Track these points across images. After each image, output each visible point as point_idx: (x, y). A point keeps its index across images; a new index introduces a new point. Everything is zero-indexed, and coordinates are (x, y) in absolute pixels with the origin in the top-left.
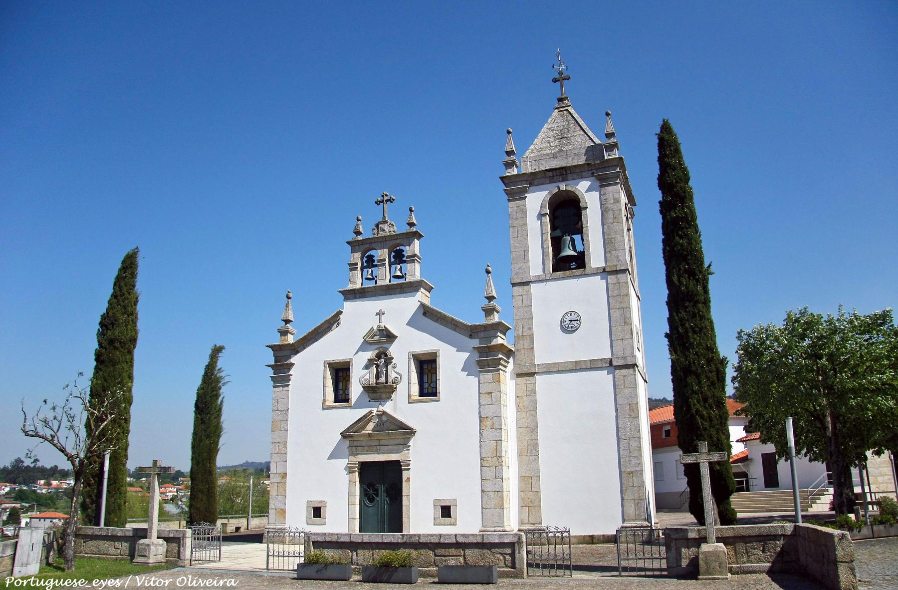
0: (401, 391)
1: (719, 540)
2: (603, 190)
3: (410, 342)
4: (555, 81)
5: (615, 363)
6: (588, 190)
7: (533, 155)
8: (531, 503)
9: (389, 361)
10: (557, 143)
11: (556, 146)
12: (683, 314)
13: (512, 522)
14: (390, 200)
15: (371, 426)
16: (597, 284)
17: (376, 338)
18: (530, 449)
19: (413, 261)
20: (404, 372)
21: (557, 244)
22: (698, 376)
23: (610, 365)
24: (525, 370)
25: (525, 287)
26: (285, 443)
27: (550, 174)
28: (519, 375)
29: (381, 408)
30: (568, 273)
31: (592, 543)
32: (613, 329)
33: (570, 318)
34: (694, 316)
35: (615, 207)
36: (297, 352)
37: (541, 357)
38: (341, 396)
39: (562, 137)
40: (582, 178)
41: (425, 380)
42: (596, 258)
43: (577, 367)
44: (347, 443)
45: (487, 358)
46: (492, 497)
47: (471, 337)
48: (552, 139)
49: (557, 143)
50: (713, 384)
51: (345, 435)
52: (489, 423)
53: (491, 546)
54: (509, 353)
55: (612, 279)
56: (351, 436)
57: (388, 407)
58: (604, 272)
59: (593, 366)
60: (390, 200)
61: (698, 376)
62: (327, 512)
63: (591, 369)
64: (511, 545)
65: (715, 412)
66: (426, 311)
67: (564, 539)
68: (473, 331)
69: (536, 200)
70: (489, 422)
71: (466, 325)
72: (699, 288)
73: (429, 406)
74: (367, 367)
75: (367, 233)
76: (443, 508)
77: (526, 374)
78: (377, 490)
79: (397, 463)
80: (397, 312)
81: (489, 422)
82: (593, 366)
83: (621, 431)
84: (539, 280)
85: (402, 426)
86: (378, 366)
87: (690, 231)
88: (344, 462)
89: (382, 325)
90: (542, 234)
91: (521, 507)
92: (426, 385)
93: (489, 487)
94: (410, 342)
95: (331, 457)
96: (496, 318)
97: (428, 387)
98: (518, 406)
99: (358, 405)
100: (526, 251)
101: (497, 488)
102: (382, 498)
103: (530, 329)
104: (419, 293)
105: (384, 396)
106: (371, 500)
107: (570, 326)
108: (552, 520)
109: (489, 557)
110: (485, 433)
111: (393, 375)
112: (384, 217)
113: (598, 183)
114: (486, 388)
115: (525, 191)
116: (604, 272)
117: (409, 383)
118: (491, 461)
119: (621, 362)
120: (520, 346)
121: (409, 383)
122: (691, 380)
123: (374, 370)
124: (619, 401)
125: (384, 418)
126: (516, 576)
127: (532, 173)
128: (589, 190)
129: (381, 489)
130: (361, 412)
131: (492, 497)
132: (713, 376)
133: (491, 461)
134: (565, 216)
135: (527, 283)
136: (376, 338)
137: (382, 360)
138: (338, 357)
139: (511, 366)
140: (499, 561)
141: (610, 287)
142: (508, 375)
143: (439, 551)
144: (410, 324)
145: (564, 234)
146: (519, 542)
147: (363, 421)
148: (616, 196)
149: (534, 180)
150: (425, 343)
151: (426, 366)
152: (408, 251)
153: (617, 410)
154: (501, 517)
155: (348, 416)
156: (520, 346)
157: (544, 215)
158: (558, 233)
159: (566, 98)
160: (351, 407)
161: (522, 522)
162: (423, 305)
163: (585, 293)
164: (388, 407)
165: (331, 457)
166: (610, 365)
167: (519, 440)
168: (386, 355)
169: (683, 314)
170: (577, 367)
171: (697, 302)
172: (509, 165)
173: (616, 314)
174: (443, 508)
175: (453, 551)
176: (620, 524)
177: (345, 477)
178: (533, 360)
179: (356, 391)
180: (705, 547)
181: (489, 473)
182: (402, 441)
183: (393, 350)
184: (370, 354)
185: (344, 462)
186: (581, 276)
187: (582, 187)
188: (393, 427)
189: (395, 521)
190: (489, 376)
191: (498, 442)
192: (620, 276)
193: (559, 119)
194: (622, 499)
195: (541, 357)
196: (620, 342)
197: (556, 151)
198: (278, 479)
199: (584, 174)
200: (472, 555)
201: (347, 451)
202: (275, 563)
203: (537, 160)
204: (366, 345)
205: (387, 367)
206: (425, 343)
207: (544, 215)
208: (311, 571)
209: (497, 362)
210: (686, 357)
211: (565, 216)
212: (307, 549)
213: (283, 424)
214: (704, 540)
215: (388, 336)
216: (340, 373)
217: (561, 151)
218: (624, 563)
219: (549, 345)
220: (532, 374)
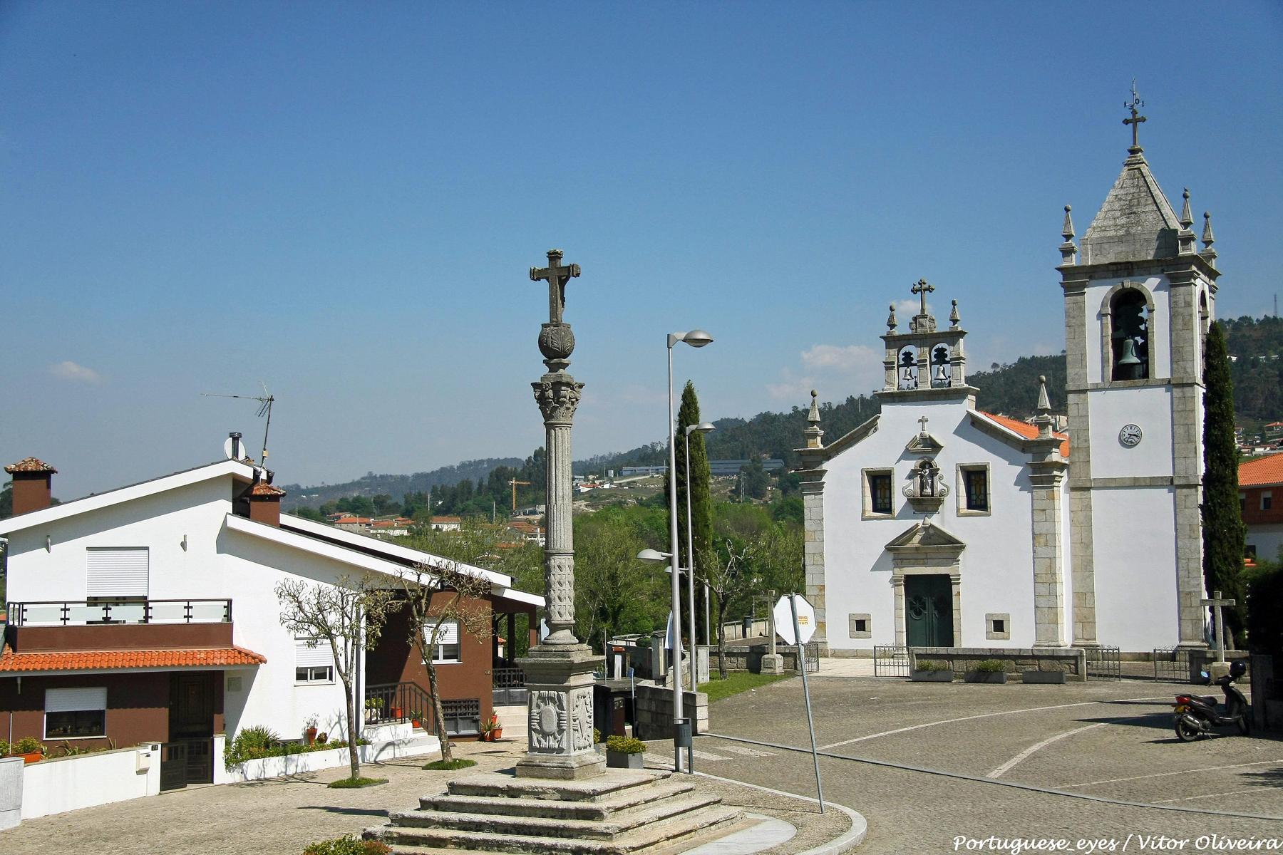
0: (949, 503)
1: (1227, 660)
2: (1174, 291)
3: (958, 453)
4: (1126, 122)
5: (1176, 482)
6: (1157, 289)
7: (1095, 236)
8: (1085, 618)
9: (934, 472)
10: (1124, 220)
11: (1122, 226)
12: (1213, 492)
13: (1066, 639)
14: (930, 289)
15: (917, 538)
16: (1161, 397)
17: (919, 447)
18: (1084, 566)
19: (958, 364)
20: (951, 483)
21: (1119, 350)
22: (1221, 541)
23: (1170, 484)
24: (1080, 484)
25: (1082, 396)
26: (822, 555)
27: (1114, 268)
28: (1073, 489)
29: (929, 521)
30: (1129, 382)
31: (1148, 660)
32: (1177, 446)
33: (1129, 431)
34: (1222, 493)
35: (1186, 312)
36: (829, 458)
37: (1098, 471)
38: (882, 504)
39: (1130, 210)
40: (1150, 274)
41: (973, 491)
42: (1161, 367)
43: (1136, 484)
44: (891, 555)
45: (1039, 475)
46: (1046, 613)
47: (1023, 451)
48: (1118, 214)
49: (1124, 220)
50: (1233, 546)
51: (890, 548)
52: (1042, 540)
53: (1059, 658)
54: (1061, 467)
55: (1177, 392)
56: (896, 551)
57: (934, 520)
58: (1169, 384)
59: (1153, 483)
60: (930, 289)
61: (1221, 541)
62: (873, 625)
63: (1150, 486)
64: (1075, 658)
65: (1233, 568)
66: (973, 421)
67: (1117, 656)
68: (1025, 446)
69: (1097, 296)
70: (1042, 539)
71: (1019, 440)
72: (1228, 472)
73: (978, 522)
74: (910, 477)
75: (902, 329)
76: (995, 622)
77: (1081, 488)
78: (924, 604)
79: (947, 576)
80: (943, 420)
81: (1042, 539)
82: (1153, 483)
83: (1180, 551)
84: (1097, 389)
85: (951, 541)
86: (922, 476)
87: (1225, 425)
88: (888, 575)
89: (927, 433)
90: (1102, 337)
91: (1075, 623)
92: (974, 497)
93: (1043, 603)
94: (958, 453)
95: (875, 568)
96: (1050, 435)
97: (977, 497)
98: (1072, 521)
99: (902, 516)
100: (1084, 355)
101: (1051, 604)
102: (931, 611)
103: (1087, 441)
104: (966, 401)
105: (930, 508)
106: (918, 613)
107: (1130, 440)
108: (1105, 638)
109: (1058, 666)
110: (1038, 550)
111: (939, 487)
112: (923, 310)
113: (1168, 283)
114: (1038, 505)
115: (1084, 285)
116: (1169, 384)
117: (958, 496)
118: (1045, 578)
119: (1182, 482)
120: (1075, 458)
121: (958, 496)
122: (1215, 543)
123: (918, 479)
124: (1180, 521)
125: (931, 531)
126: (1079, 680)
127: (1092, 266)
128: (1157, 289)
129: (929, 602)
130: (908, 524)
131: (1046, 613)
132: (1234, 541)
133: (1045, 578)
134: (1127, 314)
135: (1084, 391)
136: (919, 447)
137: (926, 471)
138: (878, 465)
139: (1064, 480)
140: (1065, 668)
141: (1176, 401)
142: (1062, 489)
143: (1019, 661)
144: (957, 432)
145: (1127, 337)
146: (1081, 656)
147: (910, 533)
148: (1188, 299)
149: (1095, 273)
150: (975, 454)
151: (975, 479)
152: (950, 352)
153: (1176, 530)
154: (1055, 632)
155: (892, 528)
156: (1075, 458)
157: (1106, 315)
158: (1121, 333)
159: (1140, 150)
160: (893, 518)
161: (1075, 638)
162: (969, 415)
163: (1147, 406)
164: (934, 520)
165: (875, 568)
166: (1170, 484)
167: (1073, 555)
168: (931, 466)
169: (1213, 492)
170: (1136, 484)
171: (1224, 484)
172: (1067, 252)
173: (1180, 431)
174: (995, 622)
175: (1030, 661)
176: (1177, 643)
177: (890, 591)
178: (1089, 473)
179: (899, 501)
180: (1215, 664)
181: (1043, 589)
182: (951, 555)
183: (939, 460)
184: (912, 464)
185: (888, 575)
186: (1144, 387)
187: (1150, 285)
188: (942, 540)
189: (946, 635)
190: (1042, 493)
191: (1052, 559)
192: (1187, 389)
193: (1129, 182)
194: (1180, 619)
195: (1098, 471)
196: (1182, 461)
197: (1121, 232)
198: (816, 592)
199: (1153, 270)
200: (1045, 664)
201: (891, 564)
202: (882, 671)
203: (1099, 244)
204: (908, 454)
205: (932, 478)
206: (975, 454)
207: (1106, 315)
208: (923, 675)
209: (1052, 479)
210: (1213, 526)
211: (1127, 314)
212: (912, 660)
213: (817, 535)
214: (1215, 659)
215: (935, 447)
216: (880, 482)
217: (1128, 233)
218: (1159, 676)
219: (1105, 460)
220: (1089, 489)
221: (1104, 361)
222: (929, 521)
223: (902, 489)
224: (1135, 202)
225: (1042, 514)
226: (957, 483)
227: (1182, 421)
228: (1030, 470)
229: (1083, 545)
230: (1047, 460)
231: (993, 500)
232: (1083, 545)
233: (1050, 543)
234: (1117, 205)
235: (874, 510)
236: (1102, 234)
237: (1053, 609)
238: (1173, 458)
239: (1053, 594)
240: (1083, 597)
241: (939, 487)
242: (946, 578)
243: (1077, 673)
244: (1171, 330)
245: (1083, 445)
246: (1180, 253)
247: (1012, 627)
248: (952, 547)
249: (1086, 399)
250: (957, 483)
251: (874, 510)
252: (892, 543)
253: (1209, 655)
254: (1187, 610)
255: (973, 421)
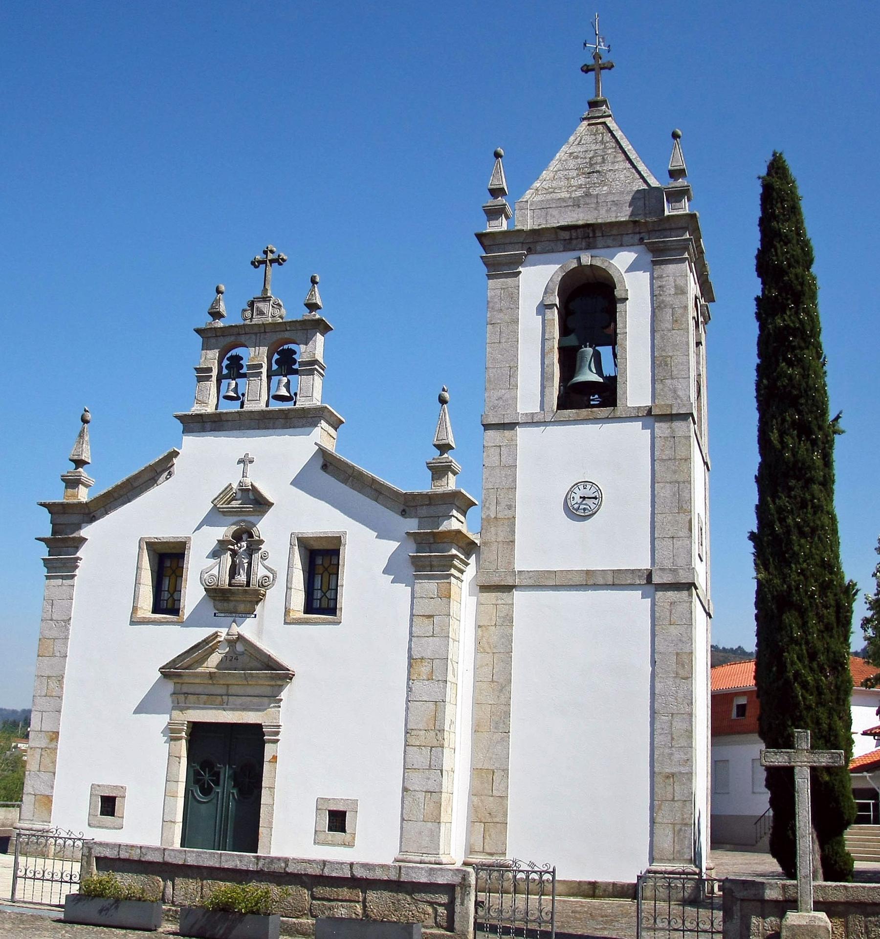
1: (818, 906)
2: (658, 270)
3: (296, 515)
5: (656, 580)
8: (489, 816)
9: (254, 546)
10: (582, 180)
11: (580, 187)
12: (784, 501)
13: (454, 849)
14: (279, 261)
15: (214, 659)
16: (636, 435)
18: (494, 723)
19: (311, 372)
21: (569, 360)
22: (802, 613)
24: (495, 580)
26: (60, 679)
27: (566, 235)
28: (485, 588)
29: (235, 629)
30: (584, 412)
31: (593, 896)
32: (658, 518)
33: (581, 492)
34: (803, 505)
35: (677, 302)
36: (92, 519)
37: (526, 559)
38: (166, 602)
39: (591, 170)
41: (318, 584)
42: (636, 391)
43: (589, 581)
44: (170, 686)
45: (430, 554)
46: (421, 801)
47: (404, 513)
48: (575, 173)
49: (582, 180)
50: (828, 628)
51: (169, 672)
52: (424, 669)
55: (662, 428)
57: (247, 629)
59: (617, 581)
61: (802, 613)
63: (614, 586)
64: (449, 889)
66: (326, 462)
68: (408, 504)
70: (425, 667)
72: (816, 456)
73: (320, 632)
74: (215, 554)
75: (232, 316)
77: (496, 587)
78: (217, 774)
79: (259, 727)
81: (425, 667)
82: (617, 581)
83: (659, 700)
84: (532, 422)
85: (270, 664)
86: (234, 554)
88: (162, 720)
89: (248, 481)
90: (544, 340)
91: (471, 823)
92: (318, 594)
93: (417, 782)
94: (296, 515)
99: (195, 621)
100: (513, 369)
102: (226, 790)
103: (511, 507)
104: (317, 431)
105: (241, 607)
106: (206, 791)
107: (581, 507)
108: (522, 850)
110: (417, 686)
112: (265, 290)
113: (649, 257)
114: (423, 607)
115: (519, 261)
117: (288, 589)
118: (424, 737)
119: (667, 579)
120: (491, 537)
121: (288, 589)
122: (790, 618)
123: (227, 559)
124: (659, 647)
125: (240, 647)
127: (533, 231)
131: (421, 801)
132: (829, 614)
133: (424, 737)
134: (588, 311)
135: (511, 426)
136: (235, 504)
137: (243, 543)
142: (465, 586)
143: (319, 891)
144: (296, 483)
145: (583, 343)
146: (464, 884)
150: (322, 518)
152: (302, 353)
153: (653, 663)
154: (435, 837)
155: (175, 639)
156: (491, 537)
157: (550, 306)
158: (572, 340)
159: (604, 102)
160: (181, 623)
161: (470, 850)
162: (322, 452)
163: (611, 451)
164: (247, 629)
166: (648, 582)
167: (477, 703)
170: (589, 581)
171: (811, 480)
172: (494, 213)
173: (665, 492)
175: (345, 892)
177: (162, 747)
178: (511, 562)
179: (192, 594)
180: (792, 918)
181: (420, 758)
182: (267, 691)
183: (265, 527)
184: (222, 532)
185: (162, 720)
187: (621, 262)
190: (430, 586)
191: (439, 704)
192: (678, 425)
193: (589, 139)
195: (526, 559)
196: (669, 542)
199: (626, 239)
201: (169, 701)
203: (544, 208)
206: (322, 518)
207: (550, 306)
208: (90, 909)
209: (447, 563)
210: (784, 578)
211: (588, 311)
214: (792, 904)
217: (587, 195)
219: (541, 539)
221: (545, 377)
222: (235, 629)
223: (200, 571)
224: (599, 159)
225: (428, 622)
226: (290, 567)
227: (669, 477)
228: (414, 546)
229: (496, 685)
230: (442, 528)
231: (347, 598)
232: (496, 685)
233: (437, 675)
234: (572, 164)
235: (155, 611)
236: (548, 197)
237: (434, 793)
238: (653, 539)
239: (436, 768)
240: (490, 778)
241: (260, 572)
242: (256, 730)
243: (450, 927)
244: (653, 331)
245: (504, 514)
246: (667, 213)
247: (359, 823)
248: (273, 675)
249: (512, 445)
250: (290, 567)
251: (155, 611)
252: (173, 664)
253: (772, 894)
254: (666, 807)
255: (326, 462)
